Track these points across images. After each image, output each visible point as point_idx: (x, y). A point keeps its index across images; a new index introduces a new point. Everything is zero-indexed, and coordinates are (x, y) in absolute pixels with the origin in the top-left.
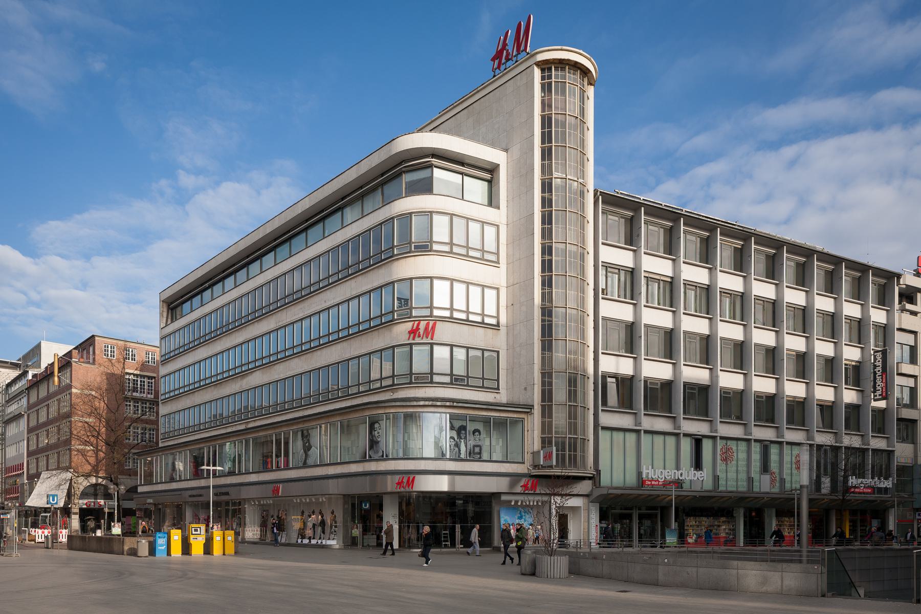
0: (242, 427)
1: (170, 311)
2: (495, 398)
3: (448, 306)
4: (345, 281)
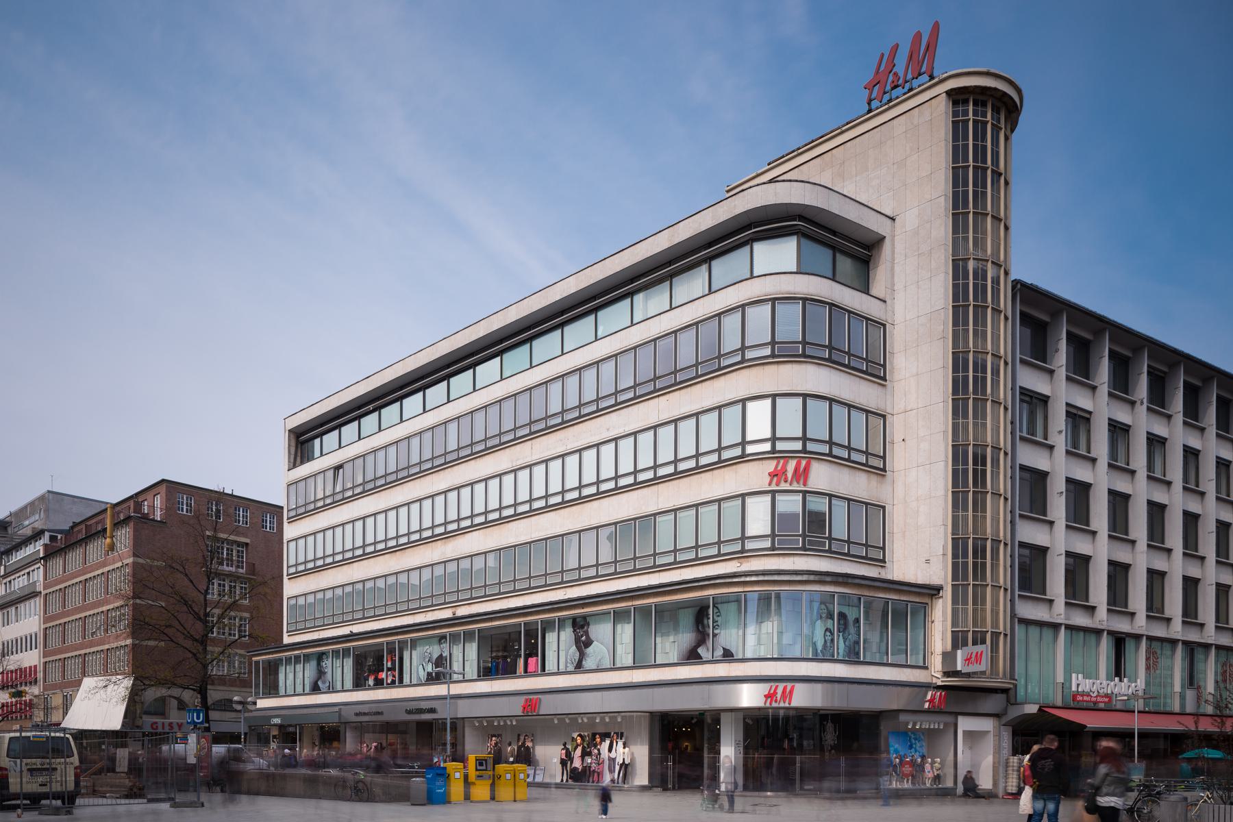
0: (446, 614)
1: (299, 446)
2: (880, 573)
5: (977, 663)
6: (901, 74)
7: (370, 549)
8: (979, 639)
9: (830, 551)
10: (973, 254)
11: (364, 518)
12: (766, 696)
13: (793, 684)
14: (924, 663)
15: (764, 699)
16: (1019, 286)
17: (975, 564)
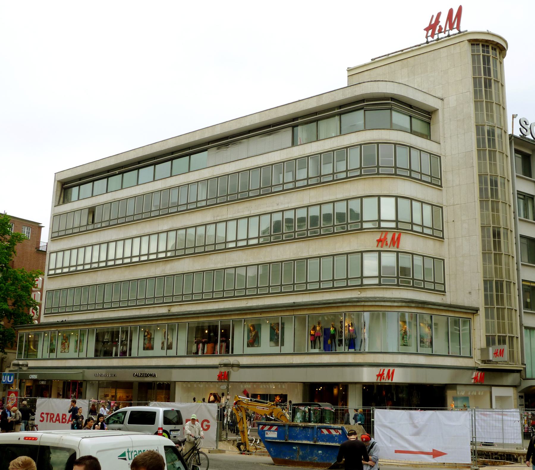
0: (163, 310)
1: (63, 191)
2: (442, 299)
4: (304, 190)
5: (501, 356)
6: (443, 27)
7: (111, 263)
8: (502, 340)
9: (413, 287)
10: (487, 122)
11: (108, 243)
12: (378, 376)
13: (394, 368)
14: (471, 355)
15: (376, 377)
16: (513, 138)
17: (497, 296)
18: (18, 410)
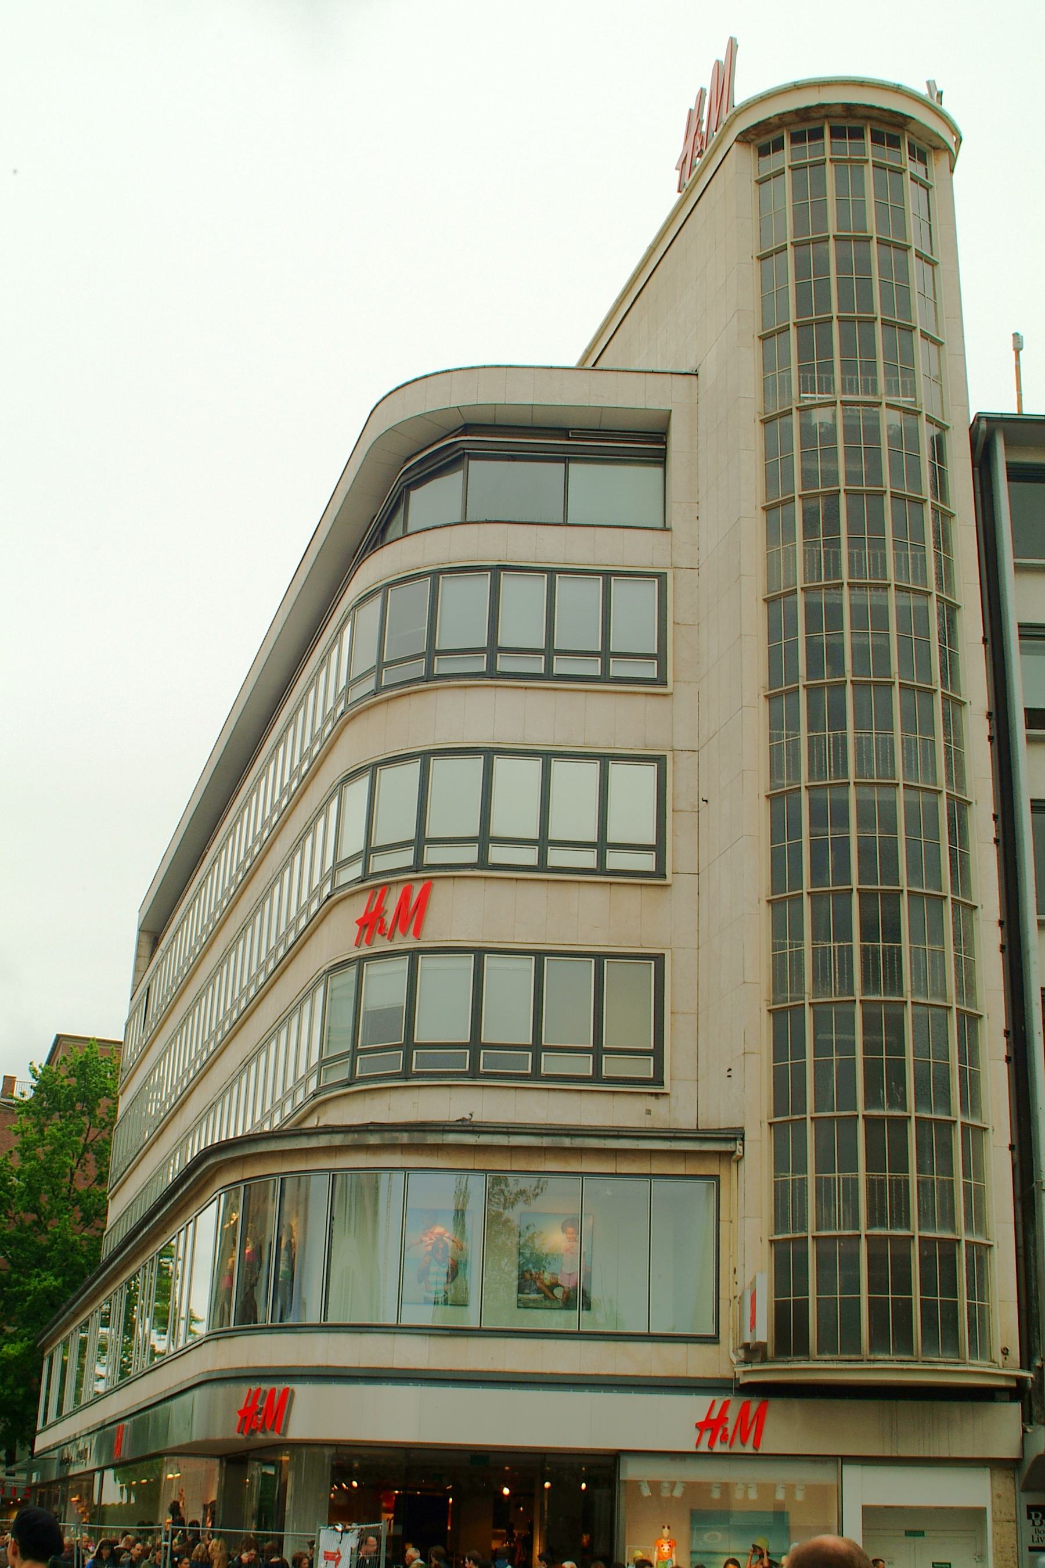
2: (649, 1112)
3: (592, 836)
12: (701, 1427)
13: (727, 1398)
15: (697, 1433)
18: (63, 1555)
